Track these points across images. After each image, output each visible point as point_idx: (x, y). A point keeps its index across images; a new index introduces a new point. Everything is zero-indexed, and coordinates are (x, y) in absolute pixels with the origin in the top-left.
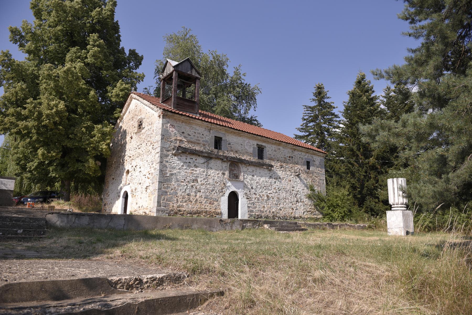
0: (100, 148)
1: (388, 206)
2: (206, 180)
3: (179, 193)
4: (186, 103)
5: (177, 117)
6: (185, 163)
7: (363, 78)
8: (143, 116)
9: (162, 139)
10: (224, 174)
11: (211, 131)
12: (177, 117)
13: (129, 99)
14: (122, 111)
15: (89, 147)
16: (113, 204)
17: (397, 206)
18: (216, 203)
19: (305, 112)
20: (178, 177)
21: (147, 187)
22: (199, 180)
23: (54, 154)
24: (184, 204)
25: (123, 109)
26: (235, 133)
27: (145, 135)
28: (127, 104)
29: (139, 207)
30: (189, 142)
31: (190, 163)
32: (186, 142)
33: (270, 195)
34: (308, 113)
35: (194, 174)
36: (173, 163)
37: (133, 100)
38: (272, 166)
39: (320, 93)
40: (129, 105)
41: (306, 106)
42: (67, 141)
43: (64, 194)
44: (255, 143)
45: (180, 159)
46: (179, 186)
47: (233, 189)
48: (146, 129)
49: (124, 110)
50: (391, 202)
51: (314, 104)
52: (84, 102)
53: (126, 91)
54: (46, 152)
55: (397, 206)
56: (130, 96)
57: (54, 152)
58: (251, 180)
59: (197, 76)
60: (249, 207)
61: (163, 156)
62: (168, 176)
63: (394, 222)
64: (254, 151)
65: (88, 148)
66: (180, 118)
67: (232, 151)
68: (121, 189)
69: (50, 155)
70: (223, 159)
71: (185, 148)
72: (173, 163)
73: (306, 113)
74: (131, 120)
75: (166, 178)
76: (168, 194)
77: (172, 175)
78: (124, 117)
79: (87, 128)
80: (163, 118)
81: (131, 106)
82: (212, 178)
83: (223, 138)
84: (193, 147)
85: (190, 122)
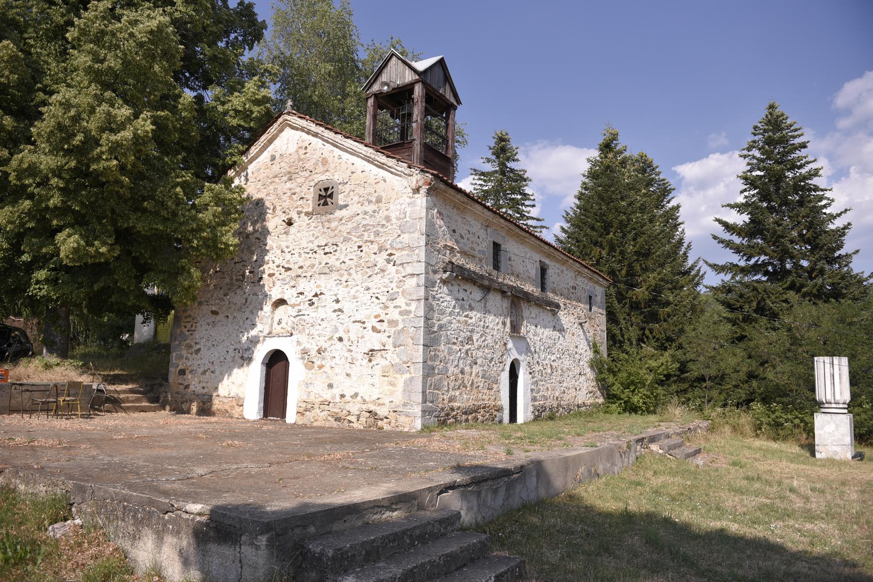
0: (222, 243)
1: (817, 406)
2: (483, 338)
3: (451, 369)
4: (437, 160)
5: (450, 195)
6: (457, 299)
7: (614, 137)
8: (337, 177)
9: (427, 244)
10: (504, 324)
11: (489, 230)
12: (450, 195)
13: (276, 125)
14: (248, 149)
15: (196, 239)
16: (222, 375)
17: (838, 406)
18: (495, 386)
19: (474, 182)
20: (449, 333)
21: (372, 350)
22: (475, 338)
23: (103, 250)
24: (457, 393)
25: (253, 148)
26: (518, 236)
27: (350, 225)
28: (264, 138)
29: (343, 396)
30: (463, 253)
31: (463, 300)
32: (458, 252)
33: (554, 364)
34: (481, 185)
35: (469, 325)
36: (441, 300)
37: (288, 130)
38: (558, 306)
39: (503, 150)
40: (270, 141)
41: (475, 170)
42: (133, 217)
43: (57, 340)
44: (537, 257)
45: (451, 292)
46: (450, 354)
47: (517, 356)
48: (354, 208)
49: (254, 150)
50: (820, 395)
51: (489, 168)
52: (166, 118)
53: (268, 105)
54: (82, 242)
55: (838, 406)
56: (280, 120)
57: (104, 243)
58: (534, 335)
59: (452, 100)
60: (532, 390)
61: (429, 285)
62: (436, 332)
63: (830, 433)
64: (536, 274)
65: (196, 242)
66: (454, 197)
67: (513, 274)
68: (254, 341)
69: (91, 250)
70: (505, 292)
71: (461, 268)
72: (441, 300)
73: (476, 184)
74: (285, 178)
75: (432, 336)
76: (436, 371)
77: (441, 327)
78: (251, 168)
79: (184, 185)
80: (429, 193)
81: (277, 142)
82: (491, 334)
83: (502, 246)
84: (467, 263)
85: (465, 208)
